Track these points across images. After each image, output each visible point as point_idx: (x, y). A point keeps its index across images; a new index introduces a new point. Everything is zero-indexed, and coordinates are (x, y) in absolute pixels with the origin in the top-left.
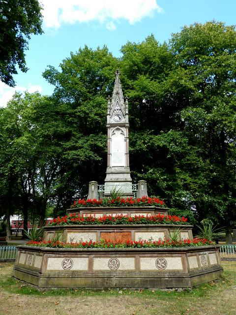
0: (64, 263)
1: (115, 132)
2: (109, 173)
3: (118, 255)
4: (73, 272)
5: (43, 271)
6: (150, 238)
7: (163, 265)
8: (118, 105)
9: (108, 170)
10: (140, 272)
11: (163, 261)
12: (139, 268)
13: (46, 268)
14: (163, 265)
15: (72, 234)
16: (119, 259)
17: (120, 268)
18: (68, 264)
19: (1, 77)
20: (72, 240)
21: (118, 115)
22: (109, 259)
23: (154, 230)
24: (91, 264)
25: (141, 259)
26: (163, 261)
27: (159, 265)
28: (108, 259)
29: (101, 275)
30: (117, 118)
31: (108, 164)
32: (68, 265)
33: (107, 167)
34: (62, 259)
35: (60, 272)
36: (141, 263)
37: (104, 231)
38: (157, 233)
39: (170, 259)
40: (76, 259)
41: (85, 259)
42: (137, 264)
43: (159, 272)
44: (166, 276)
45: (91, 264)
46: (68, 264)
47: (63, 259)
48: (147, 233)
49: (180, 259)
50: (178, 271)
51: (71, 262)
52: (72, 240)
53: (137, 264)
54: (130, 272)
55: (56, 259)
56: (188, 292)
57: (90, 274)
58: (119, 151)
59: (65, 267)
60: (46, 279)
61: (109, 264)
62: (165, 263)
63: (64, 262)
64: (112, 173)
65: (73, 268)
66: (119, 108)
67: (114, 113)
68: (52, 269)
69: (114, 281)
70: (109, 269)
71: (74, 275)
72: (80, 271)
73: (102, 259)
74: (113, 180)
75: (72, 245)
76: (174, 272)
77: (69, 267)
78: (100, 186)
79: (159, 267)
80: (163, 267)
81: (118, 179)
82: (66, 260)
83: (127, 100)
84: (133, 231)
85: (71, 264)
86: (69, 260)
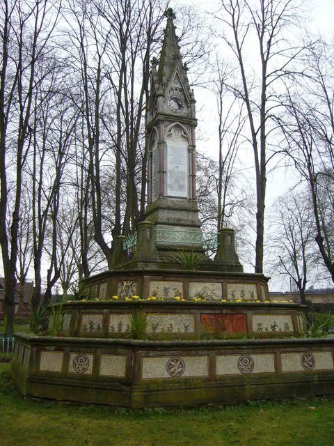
0: (169, 366)
3: (251, 351)
4: (187, 380)
6: (273, 324)
7: (310, 363)
8: (176, 81)
10: (283, 374)
12: (281, 369)
14: (310, 363)
15: (259, 317)
16: (252, 356)
17: (255, 371)
19: (64, 3)
20: (154, 328)
21: (176, 100)
22: (238, 357)
23: (278, 312)
24: (212, 366)
28: (238, 357)
30: (174, 105)
32: (176, 368)
34: (167, 359)
35: (165, 381)
36: (283, 362)
37: (207, 312)
39: (319, 354)
45: (212, 366)
51: (181, 363)
52: (154, 328)
53: (277, 364)
56: (64, 438)
57: (212, 379)
58: (179, 170)
59: (173, 373)
60: (144, 394)
61: (239, 365)
62: (313, 360)
63: (170, 364)
64: (169, 208)
65: (186, 374)
66: (178, 86)
68: (151, 376)
69: (249, 391)
70: (240, 373)
71: (188, 384)
72: (198, 378)
73: (229, 357)
74: (172, 221)
75: (155, 336)
77: (179, 373)
80: (311, 366)
81: (179, 220)
82: (173, 361)
84: (249, 313)
85: (182, 367)
86: (177, 360)
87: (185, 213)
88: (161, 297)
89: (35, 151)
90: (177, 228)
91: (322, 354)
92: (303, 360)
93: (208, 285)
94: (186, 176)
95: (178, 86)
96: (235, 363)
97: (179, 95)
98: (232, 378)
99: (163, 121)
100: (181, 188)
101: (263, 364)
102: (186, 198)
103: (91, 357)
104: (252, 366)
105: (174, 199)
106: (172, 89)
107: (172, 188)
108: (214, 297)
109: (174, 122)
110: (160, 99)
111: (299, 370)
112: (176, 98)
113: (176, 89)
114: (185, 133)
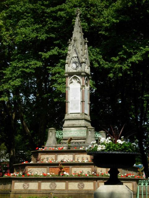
0: (24, 186)
1: (73, 80)
2: (67, 120)
5: (12, 190)
9: (67, 117)
11: (82, 184)
13: (41, 176)
18: (26, 186)
21: (75, 63)
22: (50, 183)
24: (39, 186)
25: (69, 183)
26: (82, 184)
27: (79, 187)
28: (50, 183)
29: (45, 192)
30: (74, 66)
31: (66, 111)
32: (26, 186)
33: (65, 113)
35: (21, 190)
36: (69, 186)
38: (86, 168)
40: (31, 183)
41: (36, 183)
42: (67, 186)
43: (79, 191)
44: (83, 193)
45: (39, 186)
46: (26, 186)
47: (23, 183)
48: (80, 168)
49: (93, 183)
50: (91, 190)
54: (63, 190)
55: (19, 183)
59: (25, 188)
61: (50, 186)
62: (83, 186)
63: (24, 185)
65: (30, 188)
66: (76, 55)
67: (72, 61)
68: (17, 189)
70: (50, 189)
73: (46, 183)
74: (70, 126)
76: (88, 190)
77: (27, 188)
78: (57, 132)
79: (80, 188)
80: (82, 188)
81: (74, 125)
83: (86, 44)
84: (70, 167)
87: (77, 121)
88: (80, 161)
89: (71, 60)
90: (73, 129)
91: (46, 189)
92: (79, 185)
93: (66, 156)
94: (80, 102)
95: (76, 55)
96: (49, 185)
97: (76, 60)
98: (46, 190)
99: (67, 77)
100: (77, 108)
101: (74, 186)
102: (79, 113)
103: (76, 160)
104: (56, 187)
105: (73, 114)
106: (73, 58)
107: (72, 109)
108: (68, 161)
109: (72, 76)
110: (66, 65)
111: (76, 189)
112: (76, 62)
113: (75, 57)
114: (79, 80)
